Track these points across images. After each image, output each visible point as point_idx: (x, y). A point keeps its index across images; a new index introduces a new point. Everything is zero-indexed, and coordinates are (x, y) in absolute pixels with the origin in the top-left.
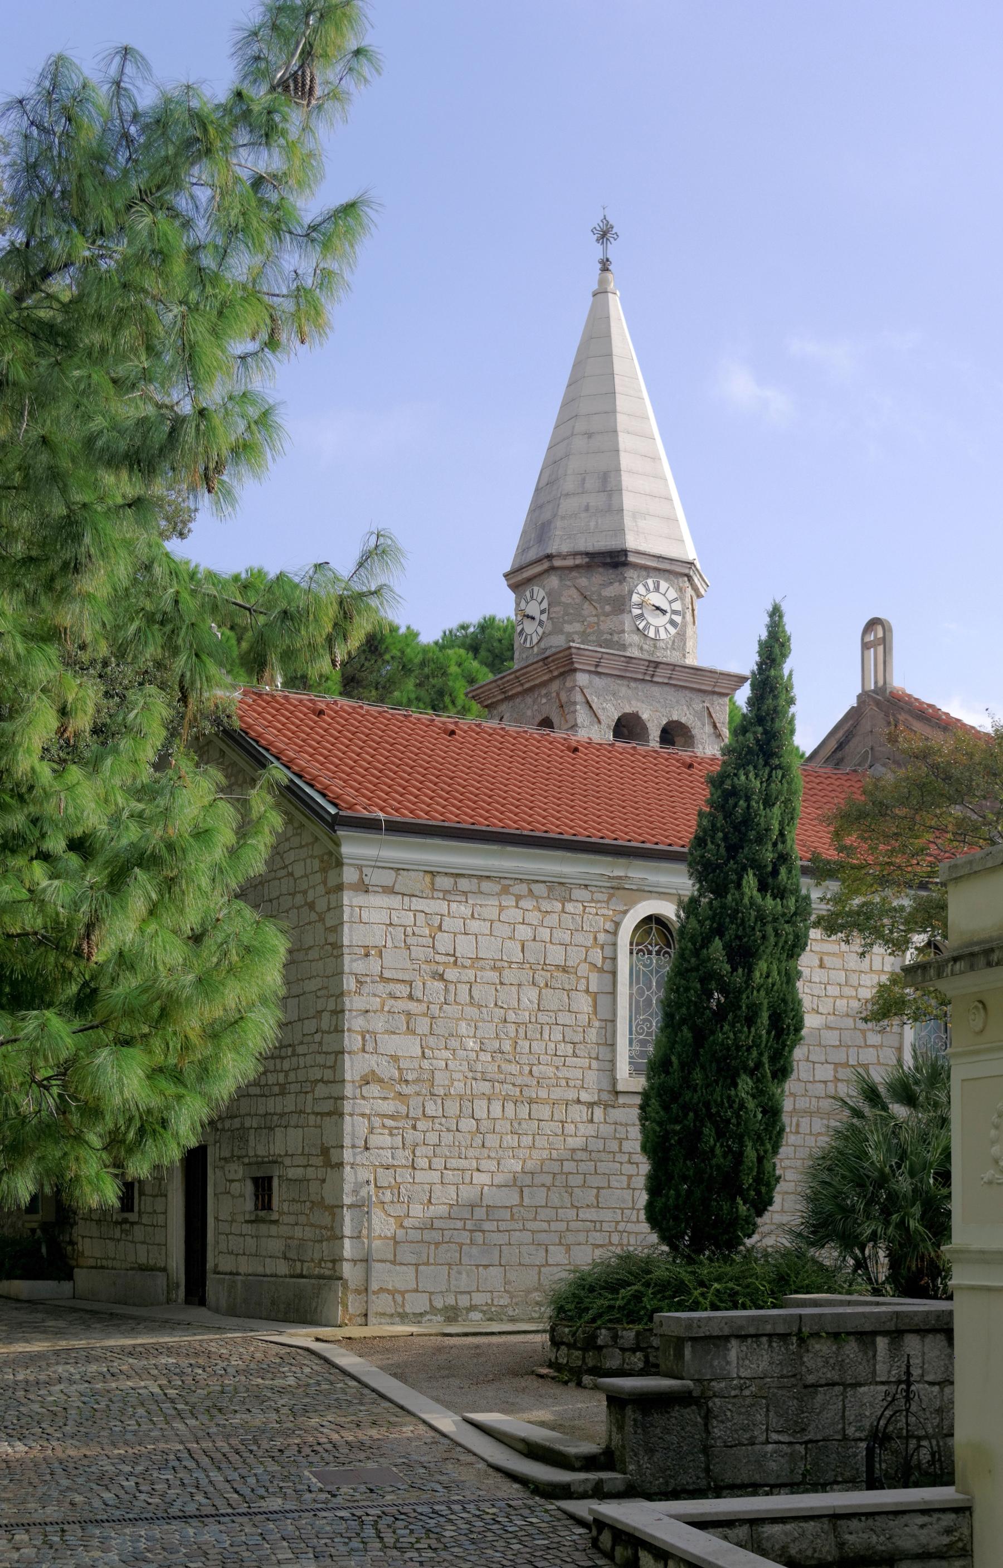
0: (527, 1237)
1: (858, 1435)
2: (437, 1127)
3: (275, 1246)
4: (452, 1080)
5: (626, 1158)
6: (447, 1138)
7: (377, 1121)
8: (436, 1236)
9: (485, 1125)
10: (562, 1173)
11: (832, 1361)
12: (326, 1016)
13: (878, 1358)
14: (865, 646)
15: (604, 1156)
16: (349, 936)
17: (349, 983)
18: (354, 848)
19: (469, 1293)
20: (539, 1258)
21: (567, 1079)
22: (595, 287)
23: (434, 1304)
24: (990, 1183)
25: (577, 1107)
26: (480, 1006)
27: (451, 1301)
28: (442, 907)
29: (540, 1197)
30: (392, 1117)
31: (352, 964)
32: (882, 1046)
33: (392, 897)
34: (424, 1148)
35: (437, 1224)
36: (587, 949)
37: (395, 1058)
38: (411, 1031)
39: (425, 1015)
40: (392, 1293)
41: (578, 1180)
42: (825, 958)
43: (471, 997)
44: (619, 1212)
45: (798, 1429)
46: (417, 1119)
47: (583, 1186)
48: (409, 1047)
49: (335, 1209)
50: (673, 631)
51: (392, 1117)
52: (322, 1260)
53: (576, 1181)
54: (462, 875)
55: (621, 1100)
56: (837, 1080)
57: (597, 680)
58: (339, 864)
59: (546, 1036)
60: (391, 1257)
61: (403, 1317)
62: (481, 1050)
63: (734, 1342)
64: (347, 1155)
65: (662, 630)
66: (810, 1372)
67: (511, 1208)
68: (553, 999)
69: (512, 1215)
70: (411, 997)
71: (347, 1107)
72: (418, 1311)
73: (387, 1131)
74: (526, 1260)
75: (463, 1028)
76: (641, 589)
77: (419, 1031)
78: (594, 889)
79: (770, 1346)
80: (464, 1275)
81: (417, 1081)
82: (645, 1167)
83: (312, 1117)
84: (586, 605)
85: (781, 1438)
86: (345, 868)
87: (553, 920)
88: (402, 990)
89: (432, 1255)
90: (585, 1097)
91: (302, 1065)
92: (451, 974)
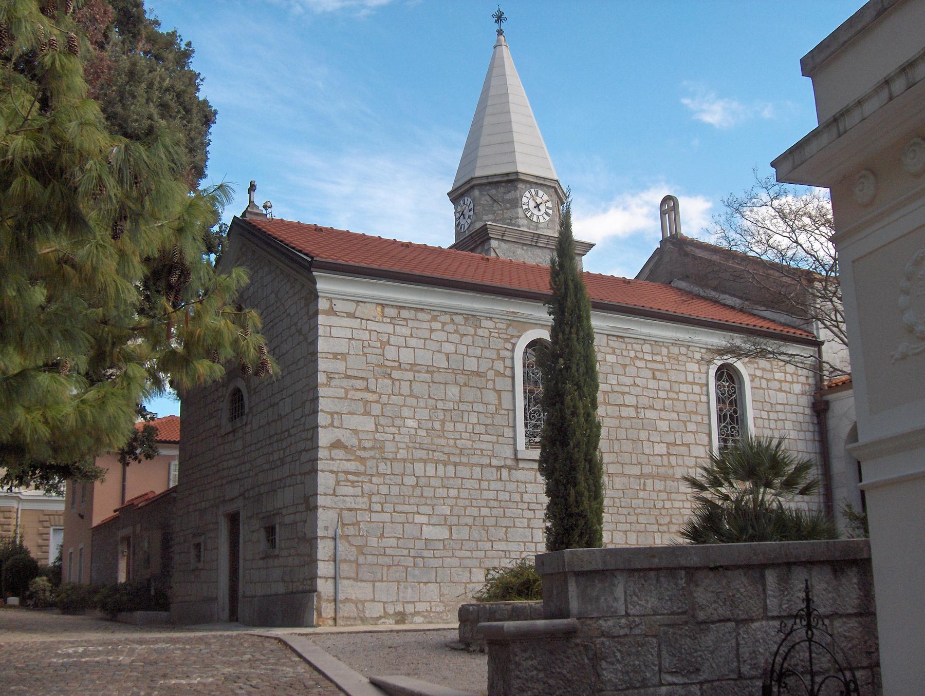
0: (455, 562)
1: (753, 673)
2: (388, 481)
4: (399, 448)
5: (526, 506)
6: (395, 490)
7: (342, 477)
8: (387, 560)
9: (423, 481)
10: (480, 516)
11: (722, 596)
12: (308, 404)
13: (769, 592)
14: (663, 213)
15: (510, 505)
16: (323, 345)
17: (322, 378)
18: (325, 285)
19: (414, 602)
20: (465, 577)
21: (482, 450)
22: (495, 43)
23: (387, 610)
24: (904, 357)
25: (490, 469)
26: (416, 397)
27: (400, 608)
28: (390, 329)
29: (464, 533)
30: (354, 474)
32: (697, 432)
33: (354, 320)
34: (378, 497)
35: (388, 551)
36: (493, 360)
37: (355, 432)
38: (367, 413)
39: (377, 402)
40: (356, 602)
41: (492, 521)
42: (656, 373)
43: (411, 390)
44: (522, 544)
45: (691, 669)
46: (372, 476)
47: (496, 526)
49: (312, 541)
50: (547, 218)
51: (354, 474)
52: (305, 579)
53: (490, 522)
54: (404, 308)
55: (521, 465)
56: (669, 454)
57: (503, 245)
58: (317, 297)
59: (466, 420)
60: (354, 575)
61: (364, 620)
62: (419, 428)
64: (321, 500)
65: (541, 218)
66: (702, 608)
67: (443, 540)
68: (470, 394)
69: (444, 546)
70: (367, 389)
71: (321, 465)
72: (375, 616)
73: (349, 484)
74: (456, 579)
75: (406, 412)
76: (527, 194)
77: (374, 413)
78: (496, 320)
79: (658, 581)
80: (409, 590)
81: (372, 448)
83: (299, 477)
84: (495, 205)
85: (675, 680)
86: (320, 300)
87: (468, 340)
88: (360, 384)
89: (385, 575)
90: (495, 462)
91: (293, 442)
92: (395, 374)
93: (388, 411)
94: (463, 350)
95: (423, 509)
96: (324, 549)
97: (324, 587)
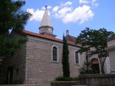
3: (18, 77)
6: (36, 66)
27: (36, 82)
31: (27, 48)
48: (33, 56)
49: (25, 72)
63: (93, 79)
64: (26, 67)
68: (46, 53)
71: (26, 62)
75: (38, 55)
82: (62, 65)
87: (46, 46)
88: (32, 51)
93: (35, 55)
94: (45, 47)
95: (40, 68)
96: (26, 73)
97: (26, 79)
